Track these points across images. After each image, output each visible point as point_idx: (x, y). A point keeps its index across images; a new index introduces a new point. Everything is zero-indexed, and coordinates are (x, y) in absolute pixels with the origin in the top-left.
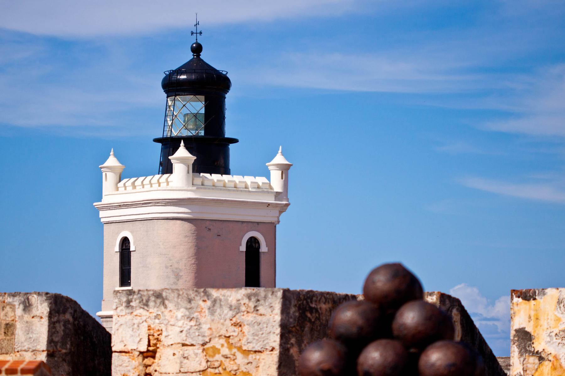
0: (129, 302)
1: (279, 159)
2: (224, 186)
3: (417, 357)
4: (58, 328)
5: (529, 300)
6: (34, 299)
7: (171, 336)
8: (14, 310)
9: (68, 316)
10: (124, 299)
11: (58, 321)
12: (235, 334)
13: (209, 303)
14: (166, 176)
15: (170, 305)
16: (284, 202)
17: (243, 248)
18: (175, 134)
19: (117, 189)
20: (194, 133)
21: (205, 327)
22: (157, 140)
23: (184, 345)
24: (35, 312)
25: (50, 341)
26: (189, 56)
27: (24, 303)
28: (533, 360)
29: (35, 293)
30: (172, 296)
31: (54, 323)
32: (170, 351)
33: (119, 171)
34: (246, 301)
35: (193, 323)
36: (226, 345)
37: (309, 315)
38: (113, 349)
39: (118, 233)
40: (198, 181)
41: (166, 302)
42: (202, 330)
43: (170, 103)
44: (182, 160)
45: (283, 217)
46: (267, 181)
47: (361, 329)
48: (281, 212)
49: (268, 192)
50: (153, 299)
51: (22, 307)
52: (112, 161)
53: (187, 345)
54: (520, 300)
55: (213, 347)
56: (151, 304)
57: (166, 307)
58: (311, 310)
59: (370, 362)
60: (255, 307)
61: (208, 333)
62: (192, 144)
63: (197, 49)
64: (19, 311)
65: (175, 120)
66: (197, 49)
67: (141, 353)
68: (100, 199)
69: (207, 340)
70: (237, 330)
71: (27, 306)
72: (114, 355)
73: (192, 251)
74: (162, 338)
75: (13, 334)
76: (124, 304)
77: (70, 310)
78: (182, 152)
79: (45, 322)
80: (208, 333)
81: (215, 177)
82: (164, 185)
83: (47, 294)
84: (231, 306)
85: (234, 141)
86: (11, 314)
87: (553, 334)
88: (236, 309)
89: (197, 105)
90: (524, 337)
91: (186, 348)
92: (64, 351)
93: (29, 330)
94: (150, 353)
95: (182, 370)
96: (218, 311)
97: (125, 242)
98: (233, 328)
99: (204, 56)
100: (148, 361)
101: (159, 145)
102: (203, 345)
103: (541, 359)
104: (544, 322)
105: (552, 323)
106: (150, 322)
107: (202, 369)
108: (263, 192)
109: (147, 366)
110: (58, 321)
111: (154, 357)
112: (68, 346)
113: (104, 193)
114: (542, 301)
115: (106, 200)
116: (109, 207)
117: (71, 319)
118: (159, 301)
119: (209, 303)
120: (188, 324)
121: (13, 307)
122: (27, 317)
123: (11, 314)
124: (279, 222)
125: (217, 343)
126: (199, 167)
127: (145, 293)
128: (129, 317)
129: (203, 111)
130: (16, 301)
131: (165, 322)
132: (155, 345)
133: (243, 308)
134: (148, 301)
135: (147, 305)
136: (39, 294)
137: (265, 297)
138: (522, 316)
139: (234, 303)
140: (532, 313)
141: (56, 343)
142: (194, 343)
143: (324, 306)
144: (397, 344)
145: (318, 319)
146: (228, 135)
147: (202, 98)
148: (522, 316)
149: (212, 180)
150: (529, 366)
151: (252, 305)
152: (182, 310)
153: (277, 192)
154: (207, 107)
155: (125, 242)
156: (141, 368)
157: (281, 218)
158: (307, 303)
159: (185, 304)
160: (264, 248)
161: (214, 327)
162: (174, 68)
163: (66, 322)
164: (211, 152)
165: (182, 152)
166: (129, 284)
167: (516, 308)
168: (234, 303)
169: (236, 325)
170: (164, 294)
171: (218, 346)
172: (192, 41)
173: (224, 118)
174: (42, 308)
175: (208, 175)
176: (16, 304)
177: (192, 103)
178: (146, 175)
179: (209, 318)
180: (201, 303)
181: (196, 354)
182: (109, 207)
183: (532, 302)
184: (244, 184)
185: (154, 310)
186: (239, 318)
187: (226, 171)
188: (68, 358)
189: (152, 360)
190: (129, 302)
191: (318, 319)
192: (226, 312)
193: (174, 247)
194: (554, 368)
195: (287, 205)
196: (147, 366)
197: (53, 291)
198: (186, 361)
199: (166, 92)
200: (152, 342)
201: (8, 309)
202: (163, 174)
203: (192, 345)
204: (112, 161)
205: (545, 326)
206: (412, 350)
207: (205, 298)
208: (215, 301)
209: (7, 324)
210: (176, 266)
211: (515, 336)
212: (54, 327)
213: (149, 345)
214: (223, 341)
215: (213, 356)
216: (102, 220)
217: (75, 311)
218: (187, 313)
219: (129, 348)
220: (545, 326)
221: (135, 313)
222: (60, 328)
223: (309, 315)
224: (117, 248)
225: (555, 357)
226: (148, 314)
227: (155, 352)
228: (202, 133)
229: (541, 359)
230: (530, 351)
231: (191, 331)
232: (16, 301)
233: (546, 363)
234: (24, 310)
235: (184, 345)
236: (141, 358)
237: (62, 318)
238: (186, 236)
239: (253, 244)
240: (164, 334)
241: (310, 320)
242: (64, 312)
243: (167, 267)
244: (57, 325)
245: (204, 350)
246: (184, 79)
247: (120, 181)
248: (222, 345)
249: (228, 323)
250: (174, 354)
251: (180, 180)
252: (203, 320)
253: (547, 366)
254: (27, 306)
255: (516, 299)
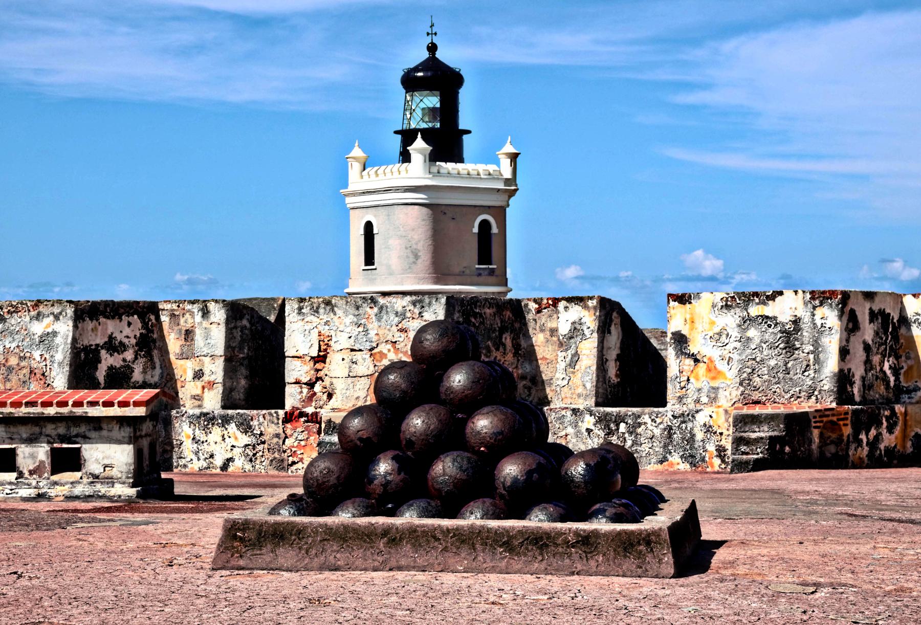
0: (300, 309)
1: (509, 148)
2: (459, 174)
3: (464, 423)
4: (235, 334)
5: (684, 304)
6: (212, 306)
7: (341, 341)
8: (193, 317)
9: (245, 322)
10: (297, 306)
11: (235, 327)
12: (401, 339)
13: (376, 310)
14: (405, 164)
15: (339, 312)
16: (513, 188)
17: (476, 230)
18: (413, 126)
19: (362, 177)
20: (430, 125)
21: (372, 333)
22: (396, 132)
23: (352, 350)
24: (212, 318)
25: (228, 347)
26: (426, 55)
27: (202, 310)
28: (689, 362)
29: (213, 300)
30: (341, 303)
31: (231, 329)
32: (339, 356)
33: (363, 161)
34: (411, 307)
35: (361, 329)
36: (392, 350)
37: (473, 320)
38: (286, 354)
39: (362, 218)
40: (434, 169)
41: (336, 309)
42: (369, 336)
43: (408, 98)
44: (420, 151)
45: (512, 201)
46: (497, 169)
47: (404, 392)
48: (510, 197)
49: (498, 179)
50: (323, 306)
51: (200, 314)
52: (357, 152)
53: (355, 350)
54: (676, 303)
55: (381, 352)
56: (321, 311)
57: (335, 314)
58: (475, 315)
59: (413, 430)
60: (420, 313)
61: (375, 338)
62: (428, 135)
63: (432, 48)
64: (198, 317)
65: (414, 114)
66: (432, 48)
67: (312, 358)
68: (346, 186)
69: (374, 345)
70: (403, 335)
71: (205, 313)
72: (287, 359)
73: (429, 233)
74: (332, 343)
75: (192, 340)
76: (296, 311)
77: (247, 316)
78: (419, 143)
79: (222, 328)
80: (375, 338)
81: (450, 166)
82: (403, 174)
83: (224, 301)
84: (397, 313)
85: (468, 132)
86: (190, 321)
87: (708, 337)
88: (402, 315)
89: (433, 101)
90: (680, 340)
91: (354, 353)
92: (241, 356)
93: (207, 337)
94: (321, 358)
95: (351, 374)
96: (385, 317)
97: (369, 226)
98: (399, 334)
99: (438, 55)
100: (318, 366)
101: (399, 137)
102: (371, 350)
103: (697, 361)
104: (699, 326)
105: (707, 326)
106: (320, 328)
107: (370, 373)
108: (494, 178)
109: (317, 370)
110: (235, 327)
111: (325, 363)
112: (246, 351)
113: (350, 181)
114: (696, 305)
115: (352, 187)
116: (354, 194)
117: (248, 325)
118: (328, 308)
119: (376, 310)
120: (356, 330)
121: (192, 314)
122: (205, 324)
123: (190, 321)
124: (508, 205)
125: (384, 348)
126: (434, 157)
127: (316, 300)
128: (301, 323)
129: (438, 105)
130: (195, 308)
131: (335, 328)
132: (325, 350)
133: (408, 315)
134: (318, 308)
135: (318, 312)
136: (216, 301)
137: (430, 304)
138: (678, 319)
139: (400, 309)
140: (688, 317)
141: (233, 349)
142: (362, 348)
143: (488, 311)
144: (442, 410)
145: (482, 323)
146: (461, 127)
147: (438, 93)
148: (678, 319)
149: (447, 168)
150: (686, 368)
151: (417, 311)
152: (351, 317)
153: (506, 179)
154: (441, 101)
155: (369, 226)
156: (312, 372)
157: (510, 202)
158: (471, 308)
159: (352, 310)
160: (495, 230)
161: (380, 333)
162: (412, 67)
163: (243, 328)
164: (446, 142)
165: (419, 143)
166: (373, 264)
167: (672, 312)
168: (400, 309)
169: (401, 330)
170: (333, 301)
171: (385, 351)
172: (428, 40)
173: (458, 111)
174: (219, 314)
175: (443, 164)
176: (196, 311)
177: (430, 98)
178: (388, 164)
179: (376, 324)
180: (368, 309)
181: (364, 359)
182: (354, 194)
183: (688, 305)
184: (476, 169)
185: (324, 316)
186: (405, 324)
187: (460, 160)
188: (246, 362)
189: (323, 364)
190: (300, 309)
191: (482, 323)
192: (392, 318)
193: (413, 230)
194: (709, 370)
195: (516, 190)
196: (317, 370)
197: (229, 298)
198: (354, 365)
199: (405, 88)
200: (323, 347)
201: (187, 315)
202: (403, 162)
203: (360, 350)
204: (357, 152)
205: (700, 329)
206: (460, 416)
207: (372, 305)
208: (381, 308)
209: (187, 331)
210: (415, 247)
211: (671, 339)
212: (232, 333)
213: (320, 351)
214: (389, 346)
215: (380, 361)
216: (348, 206)
217: (252, 317)
218: (355, 320)
219: (300, 354)
220: (700, 329)
221: (306, 320)
222: (238, 334)
223: (473, 320)
224: (362, 231)
225: (710, 359)
226: (318, 320)
227: (325, 357)
228: (438, 125)
229: (697, 361)
230: (686, 354)
231: (359, 337)
232: (195, 308)
233: (701, 365)
234: (203, 317)
235: (352, 350)
236: (312, 363)
237: (239, 324)
238: (424, 220)
239: (485, 225)
240: (334, 339)
241: (474, 325)
242: (241, 318)
243: (406, 248)
244: (234, 331)
245: (371, 355)
246: (421, 77)
247: (364, 169)
248: (389, 350)
249: (394, 329)
250: (343, 359)
251: (417, 170)
252: (370, 326)
253: (702, 367)
254: (205, 313)
255: (672, 303)
